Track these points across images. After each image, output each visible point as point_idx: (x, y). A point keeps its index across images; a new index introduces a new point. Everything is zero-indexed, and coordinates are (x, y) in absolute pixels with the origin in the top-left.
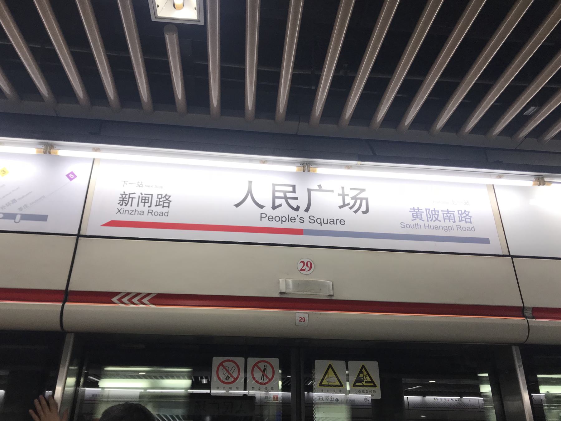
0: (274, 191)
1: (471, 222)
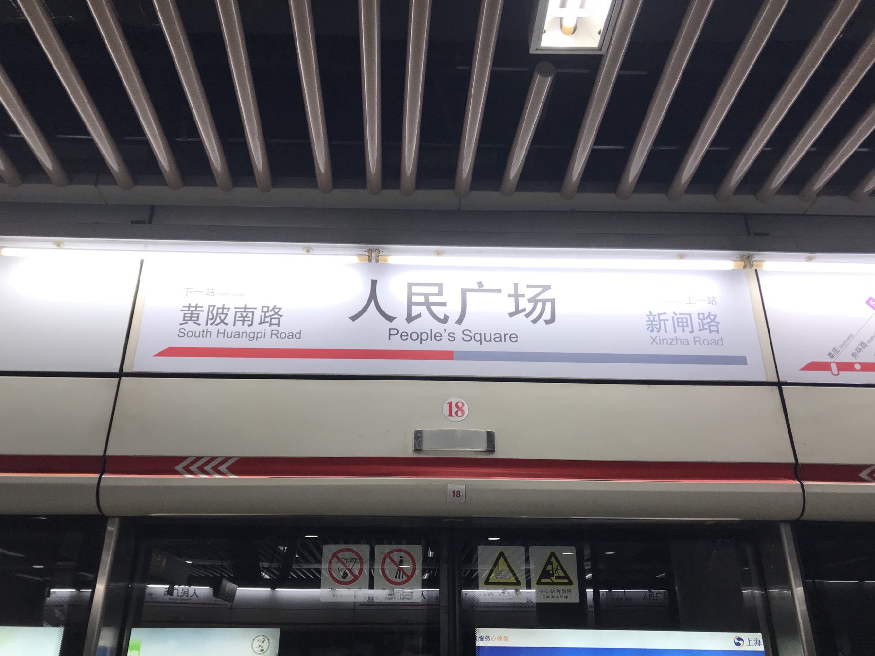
0: (410, 294)
1: (718, 331)
